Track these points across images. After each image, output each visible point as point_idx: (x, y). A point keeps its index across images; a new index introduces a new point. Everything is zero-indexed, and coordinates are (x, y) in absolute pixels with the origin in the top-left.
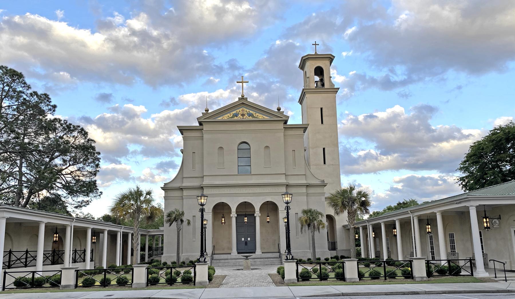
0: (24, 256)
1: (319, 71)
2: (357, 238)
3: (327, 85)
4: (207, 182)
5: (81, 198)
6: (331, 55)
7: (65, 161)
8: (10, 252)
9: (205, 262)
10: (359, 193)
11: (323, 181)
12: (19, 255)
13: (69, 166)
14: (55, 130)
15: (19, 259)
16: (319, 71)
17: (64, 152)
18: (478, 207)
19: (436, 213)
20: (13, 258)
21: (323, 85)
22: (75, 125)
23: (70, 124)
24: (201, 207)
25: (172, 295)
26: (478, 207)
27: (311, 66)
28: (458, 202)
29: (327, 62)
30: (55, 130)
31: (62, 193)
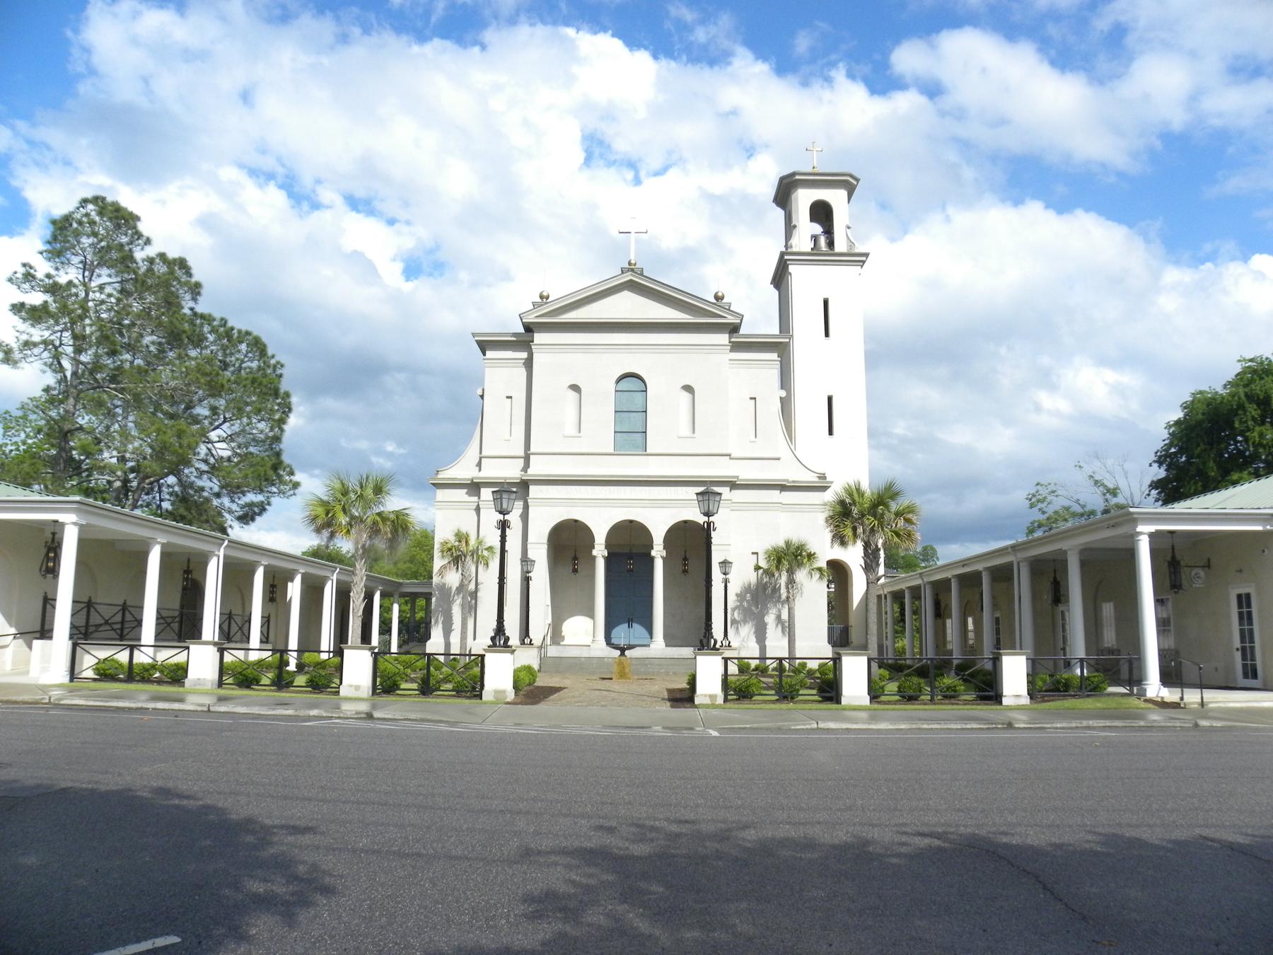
0: (118, 618)
1: (822, 213)
2: (970, 620)
3: (840, 245)
4: (538, 467)
5: (251, 497)
6: (851, 176)
7: (214, 410)
8: (89, 605)
9: (531, 644)
10: (278, 363)
11: (822, 477)
12: (107, 612)
13: (224, 422)
14: (198, 341)
15: (107, 623)
16: (822, 213)
17: (215, 389)
18: (1153, 536)
19: (1065, 552)
20: (95, 619)
21: (831, 244)
22: (244, 329)
23: (232, 329)
24: (501, 517)
25: (923, 835)
26: (1151, 535)
27: (804, 199)
28: (1111, 522)
29: (843, 193)
30: (198, 341)
31: (210, 484)
